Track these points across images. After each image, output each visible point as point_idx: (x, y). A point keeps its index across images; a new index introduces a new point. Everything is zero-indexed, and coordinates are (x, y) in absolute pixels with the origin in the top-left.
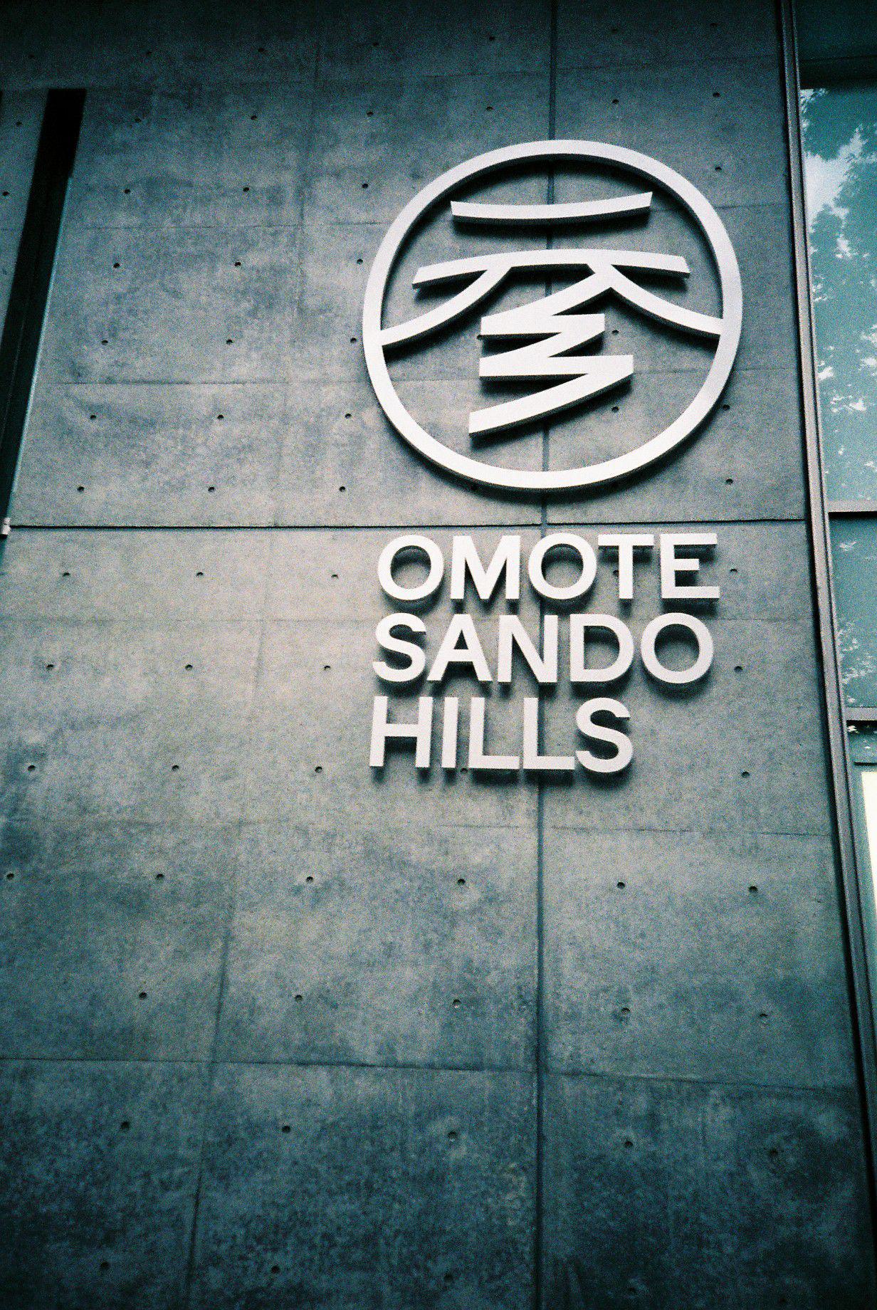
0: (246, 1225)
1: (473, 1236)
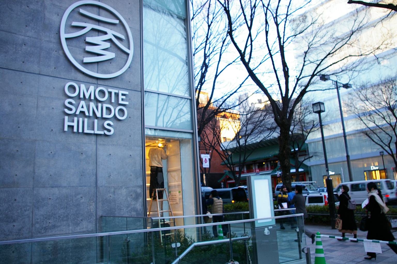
0: (43, 216)
1: (85, 213)
